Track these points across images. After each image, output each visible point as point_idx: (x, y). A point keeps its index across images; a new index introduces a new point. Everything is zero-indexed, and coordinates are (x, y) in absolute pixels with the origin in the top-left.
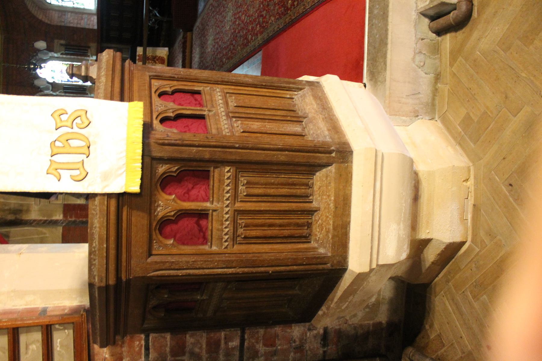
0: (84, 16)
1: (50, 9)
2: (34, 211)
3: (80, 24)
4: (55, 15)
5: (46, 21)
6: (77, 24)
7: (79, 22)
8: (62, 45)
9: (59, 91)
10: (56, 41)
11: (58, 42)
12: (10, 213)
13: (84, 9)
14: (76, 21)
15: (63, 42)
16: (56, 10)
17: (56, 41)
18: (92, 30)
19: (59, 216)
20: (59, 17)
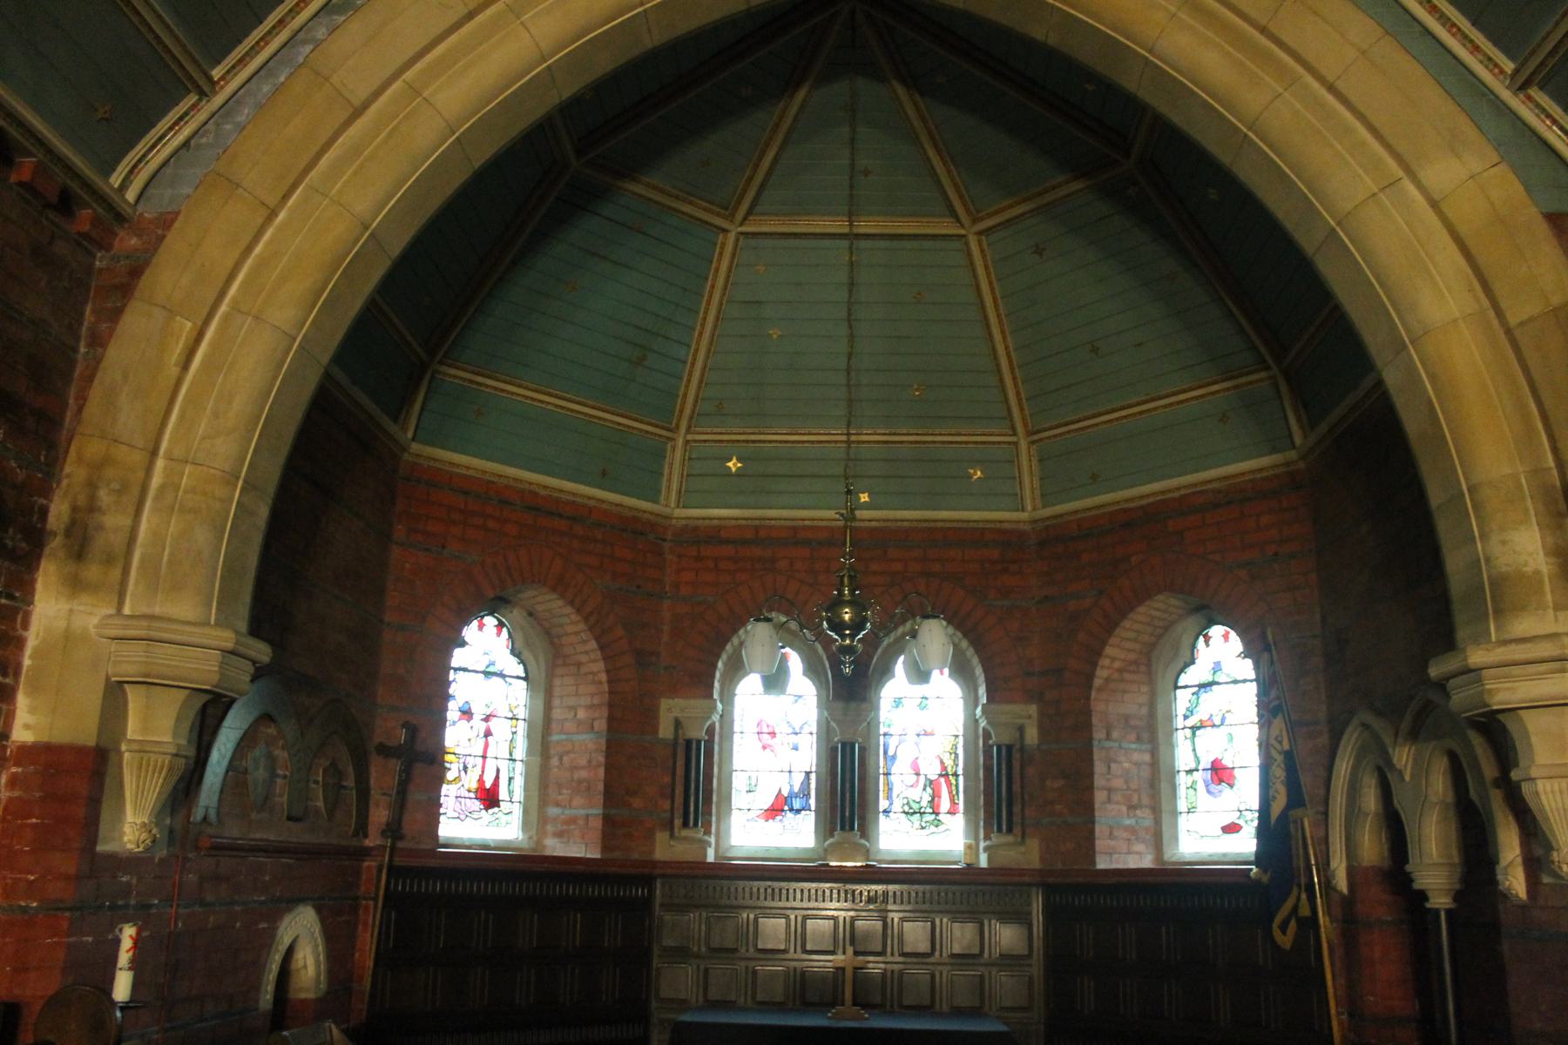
0: (1147, 821)
1: (1151, 679)
2: (71, 611)
3: (1109, 800)
4: (1132, 704)
5: (1101, 674)
6: (1110, 790)
7: (1117, 797)
8: (1021, 729)
9: (989, 728)
10: (1033, 709)
11: (1030, 717)
12: (75, 509)
13: (1175, 813)
14: (1118, 783)
15: (1032, 735)
16: (1152, 705)
17: (1033, 709)
18: (1089, 852)
19: (27, 727)
20: (1127, 718)
